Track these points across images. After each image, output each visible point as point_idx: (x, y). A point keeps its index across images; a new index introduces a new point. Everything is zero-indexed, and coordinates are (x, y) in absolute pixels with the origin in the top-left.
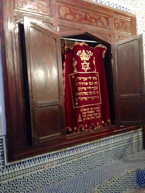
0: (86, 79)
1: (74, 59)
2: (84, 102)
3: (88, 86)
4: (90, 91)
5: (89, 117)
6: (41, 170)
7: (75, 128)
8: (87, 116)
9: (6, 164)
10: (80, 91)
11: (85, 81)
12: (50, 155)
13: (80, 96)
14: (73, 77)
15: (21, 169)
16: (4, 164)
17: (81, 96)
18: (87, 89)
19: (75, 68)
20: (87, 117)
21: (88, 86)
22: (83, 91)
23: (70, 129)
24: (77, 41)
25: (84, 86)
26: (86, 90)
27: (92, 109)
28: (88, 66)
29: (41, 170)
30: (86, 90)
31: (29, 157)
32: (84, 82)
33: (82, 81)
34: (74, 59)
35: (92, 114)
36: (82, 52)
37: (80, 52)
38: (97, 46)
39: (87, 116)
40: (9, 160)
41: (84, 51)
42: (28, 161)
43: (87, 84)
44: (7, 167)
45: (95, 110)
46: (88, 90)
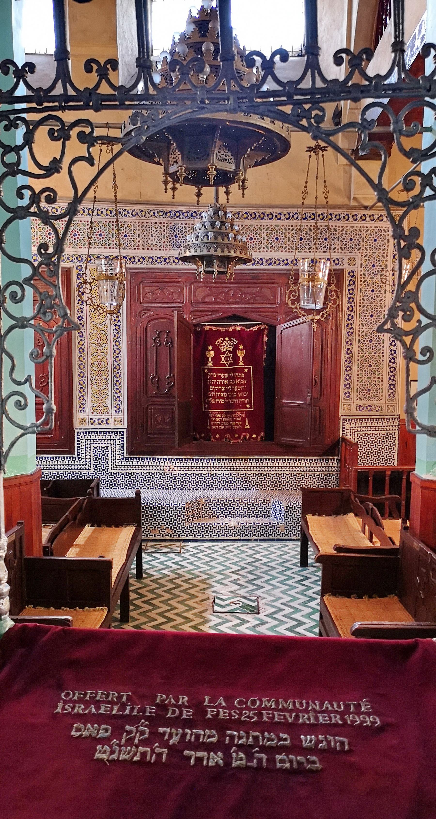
0: (226, 376)
1: (210, 348)
2: (218, 406)
3: (228, 385)
4: (230, 392)
5: (224, 425)
6: (161, 472)
7: (254, 436)
8: (221, 423)
9: (125, 456)
10: (213, 391)
11: (225, 379)
12: (172, 459)
13: (211, 397)
14: (206, 371)
15: (220, 465)
16: (123, 456)
17: (214, 397)
18: (225, 388)
19: (210, 360)
20: (220, 425)
21: (228, 385)
22: (219, 390)
23: (198, 436)
24: (208, 325)
25: (221, 385)
26: (224, 390)
27: (229, 415)
28: (223, 359)
29: (161, 472)
30: (224, 390)
31: (283, 455)
32: (223, 379)
33: (219, 378)
34: (210, 348)
35: (229, 422)
36: (224, 340)
37: (220, 340)
38: (252, 329)
39: (221, 423)
40: (129, 453)
41: (227, 339)
42: (239, 459)
43: (226, 382)
44: (126, 458)
45: (233, 418)
46: (226, 391)
